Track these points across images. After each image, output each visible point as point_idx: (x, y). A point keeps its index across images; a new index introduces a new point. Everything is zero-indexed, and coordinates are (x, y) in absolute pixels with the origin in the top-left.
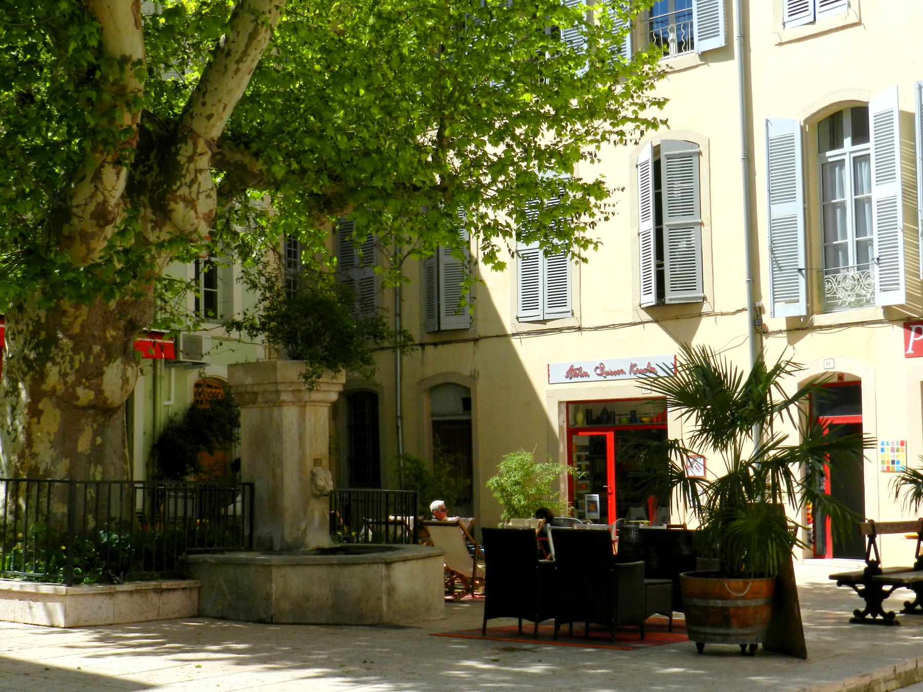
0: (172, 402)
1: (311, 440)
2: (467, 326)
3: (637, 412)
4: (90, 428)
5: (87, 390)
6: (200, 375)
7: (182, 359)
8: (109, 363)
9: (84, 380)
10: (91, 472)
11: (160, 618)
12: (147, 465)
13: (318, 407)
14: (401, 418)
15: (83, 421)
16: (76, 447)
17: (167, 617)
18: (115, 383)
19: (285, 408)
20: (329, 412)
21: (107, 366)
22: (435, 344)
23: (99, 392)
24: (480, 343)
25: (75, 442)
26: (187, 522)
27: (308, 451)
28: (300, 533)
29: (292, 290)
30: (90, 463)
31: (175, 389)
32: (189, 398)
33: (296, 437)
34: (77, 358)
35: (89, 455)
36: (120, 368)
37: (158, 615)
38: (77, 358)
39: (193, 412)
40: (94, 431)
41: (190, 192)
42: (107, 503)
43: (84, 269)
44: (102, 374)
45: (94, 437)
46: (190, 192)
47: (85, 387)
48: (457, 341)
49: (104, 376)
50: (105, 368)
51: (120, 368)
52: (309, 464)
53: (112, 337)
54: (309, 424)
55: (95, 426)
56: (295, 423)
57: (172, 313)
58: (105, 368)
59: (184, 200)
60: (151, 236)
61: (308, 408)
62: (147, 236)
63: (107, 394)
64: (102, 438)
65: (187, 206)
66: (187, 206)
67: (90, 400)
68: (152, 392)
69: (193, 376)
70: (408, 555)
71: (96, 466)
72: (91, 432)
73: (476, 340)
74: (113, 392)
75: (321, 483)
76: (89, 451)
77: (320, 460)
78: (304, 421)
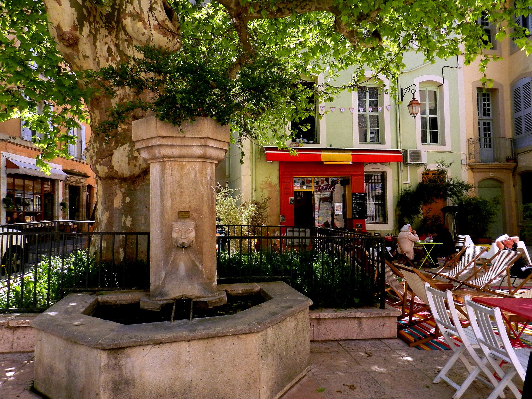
0: (409, 182)
1: (173, 194)
3: (481, 86)
4: (120, 192)
5: (102, 166)
6: (425, 169)
7: (409, 162)
8: (117, 147)
9: (99, 160)
10: (123, 221)
11: (14, 350)
12: (395, 210)
15: (114, 187)
16: (113, 204)
17: (22, 350)
18: (122, 161)
21: (115, 149)
23: (111, 167)
25: (112, 201)
27: (168, 204)
28: (161, 282)
29: (487, 127)
30: (122, 214)
32: (419, 180)
33: (159, 192)
34: (95, 145)
35: (121, 210)
36: (126, 151)
37: (12, 347)
38: (95, 145)
39: (421, 186)
40: (123, 194)
41: (134, 8)
42: (136, 241)
46: (134, 8)
50: (114, 151)
51: (126, 151)
54: (168, 179)
55: (123, 190)
56: (158, 178)
59: (132, 15)
60: (128, 52)
61: (167, 165)
62: (126, 53)
63: (116, 168)
65: (134, 20)
66: (134, 20)
68: (397, 178)
69: (421, 170)
70: (160, 336)
71: (126, 217)
72: (121, 195)
74: (120, 167)
78: (164, 176)
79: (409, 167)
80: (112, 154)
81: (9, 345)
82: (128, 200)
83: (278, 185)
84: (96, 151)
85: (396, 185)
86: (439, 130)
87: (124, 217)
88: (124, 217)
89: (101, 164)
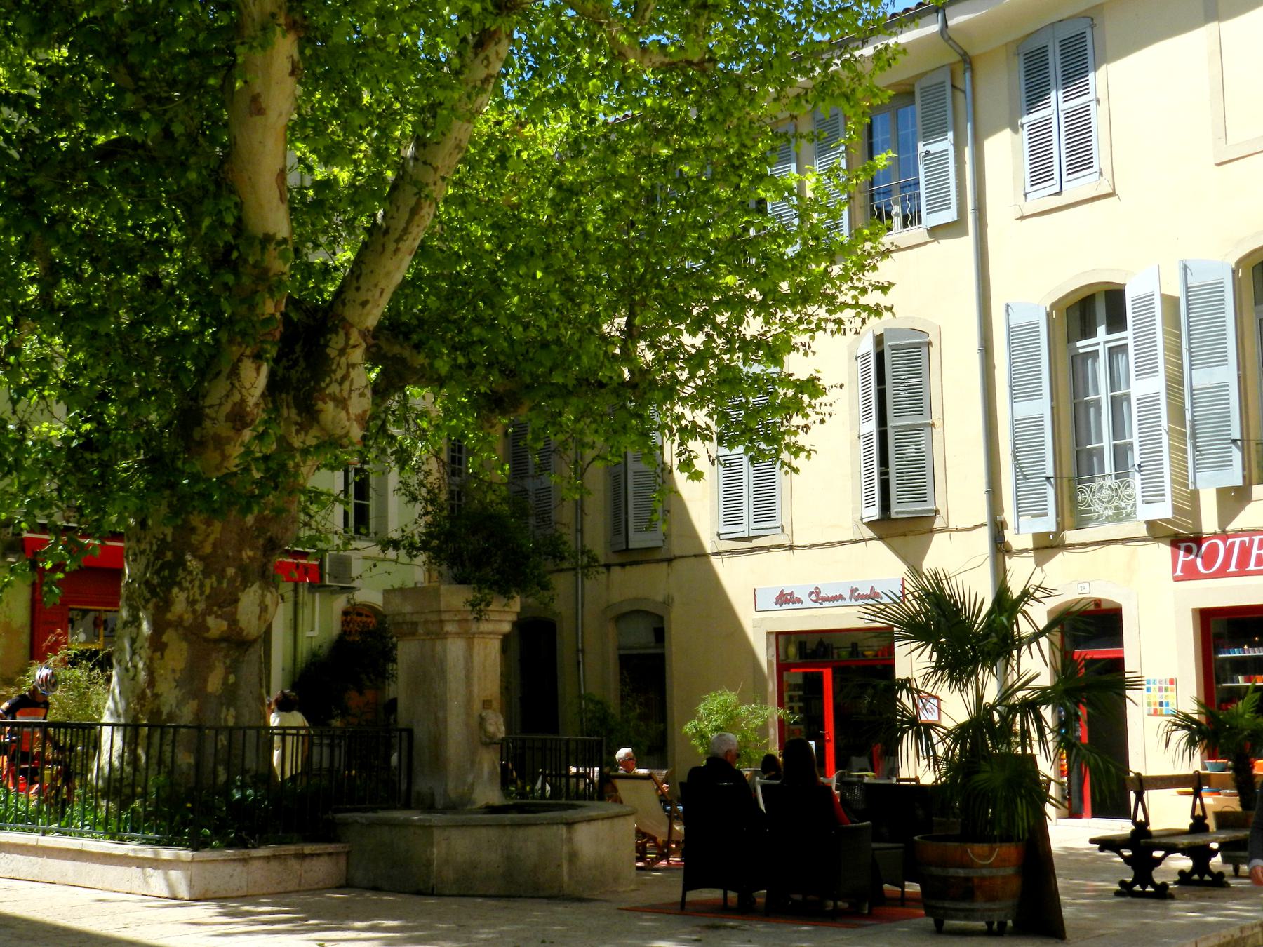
0: (315, 633)
2: (660, 544)
5: (219, 620)
6: (348, 601)
14: (583, 651)
16: (205, 687)
19: (450, 641)
21: (243, 591)
22: (623, 565)
23: (233, 622)
24: (676, 564)
27: (476, 689)
30: (222, 705)
32: (336, 629)
34: (208, 582)
35: (220, 696)
37: (299, 885)
39: (340, 645)
40: (226, 668)
48: (648, 562)
52: (477, 706)
59: (334, 398)
61: (476, 641)
69: (340, 603)
73: (670, 561)
75: (491, 729)
77: (490, 701)
79: (317, 596)
80: (236, 601)
81: (296, 881)
82: (232, 679)
83: (27, 631)
84: (208, 591)
85: (290, 642)
86: (372, 504)
87: (224, 709)
88: (224, 709)
89: (217, 617)
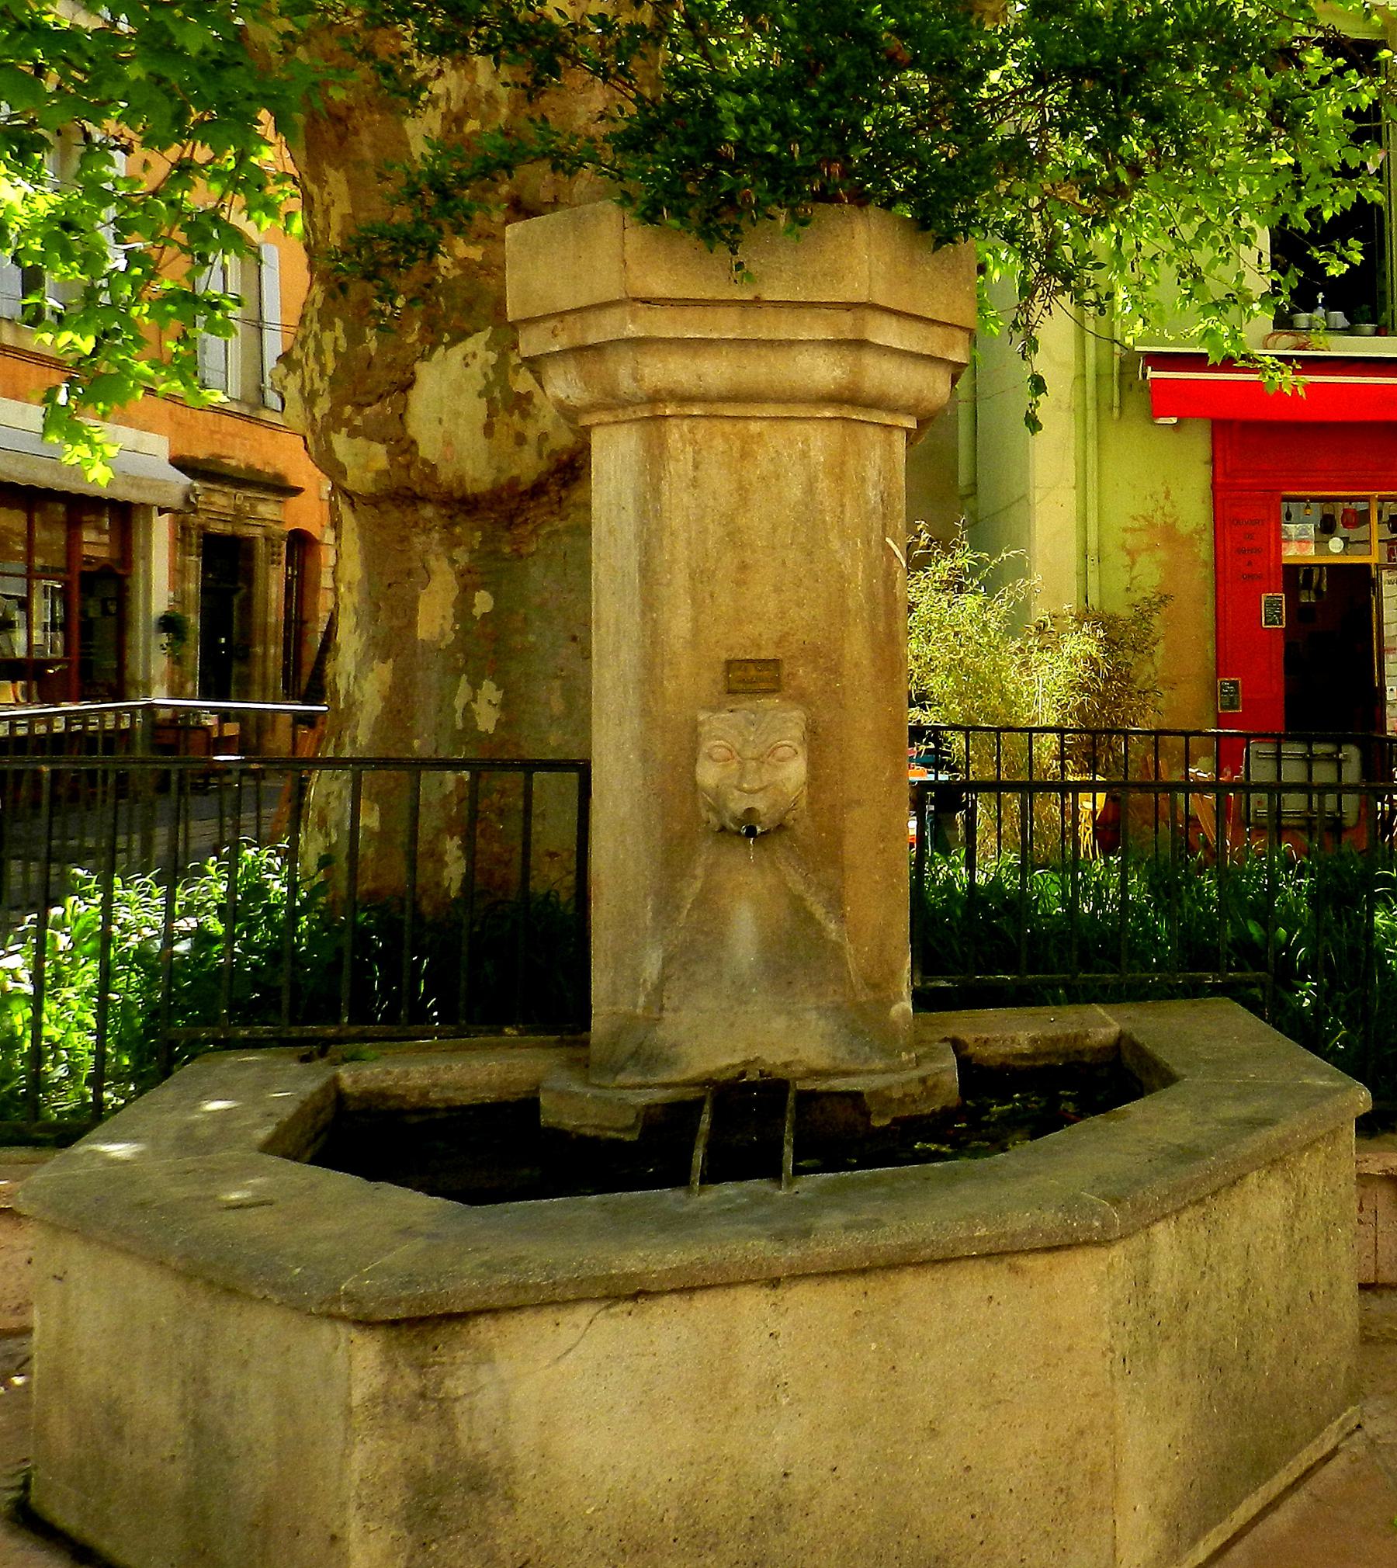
1: (700, 576)
4: (445, 564)
5: (360, 441)
10: (459, 703)
13: (754, 427)
15: (418, 541)
16: (412, 624)
20: (1026, 468)
21: (424, 357)
23: (403, 446)
25: (409, 610)
26: (160, 849)
27: (679, 623)
31: (955, 451)
33: (632, 564)
35: (450, 651)
36: (476, 367)
38: (327, 337)
40: (461, 575)
42: (521, 804)
43: (241, 28)
44: (407, 385)
45: (466, 592)
47: (354, 433)
49: (414, 395)
53: (464, 263)
54: (678, 502)
57: (519, 139)
58: (418, 366)
61: (675, 435)
63: (428, 449)
64: (496, 595)
67: (379, 473)
71: (475, 686)
72: (451, 578)
76: (451, 637)
78: (656, 492)
